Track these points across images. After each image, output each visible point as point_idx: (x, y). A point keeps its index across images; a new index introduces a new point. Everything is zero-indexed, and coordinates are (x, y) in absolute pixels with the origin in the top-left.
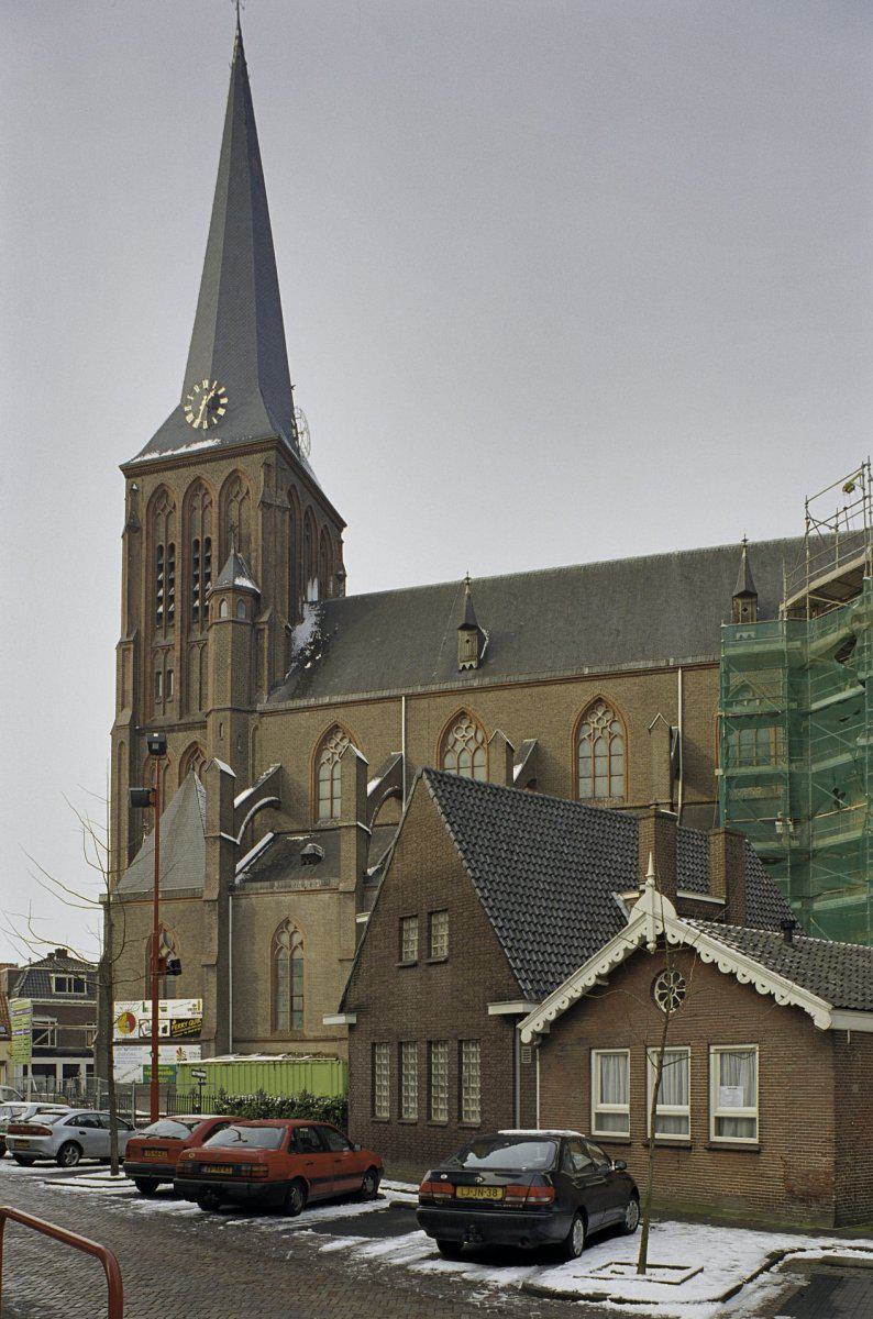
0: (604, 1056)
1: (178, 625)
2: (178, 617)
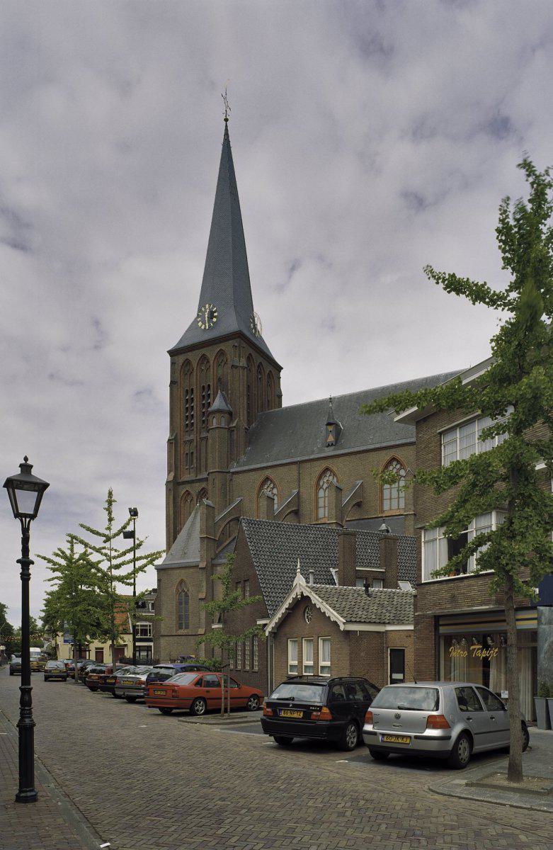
0: (307, 640)
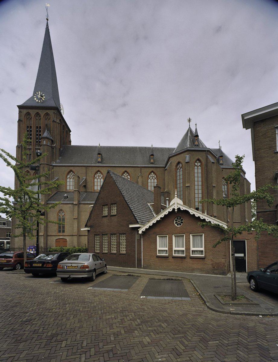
0: (159, 237)
1: (33, 144)
2: (32, 142)
